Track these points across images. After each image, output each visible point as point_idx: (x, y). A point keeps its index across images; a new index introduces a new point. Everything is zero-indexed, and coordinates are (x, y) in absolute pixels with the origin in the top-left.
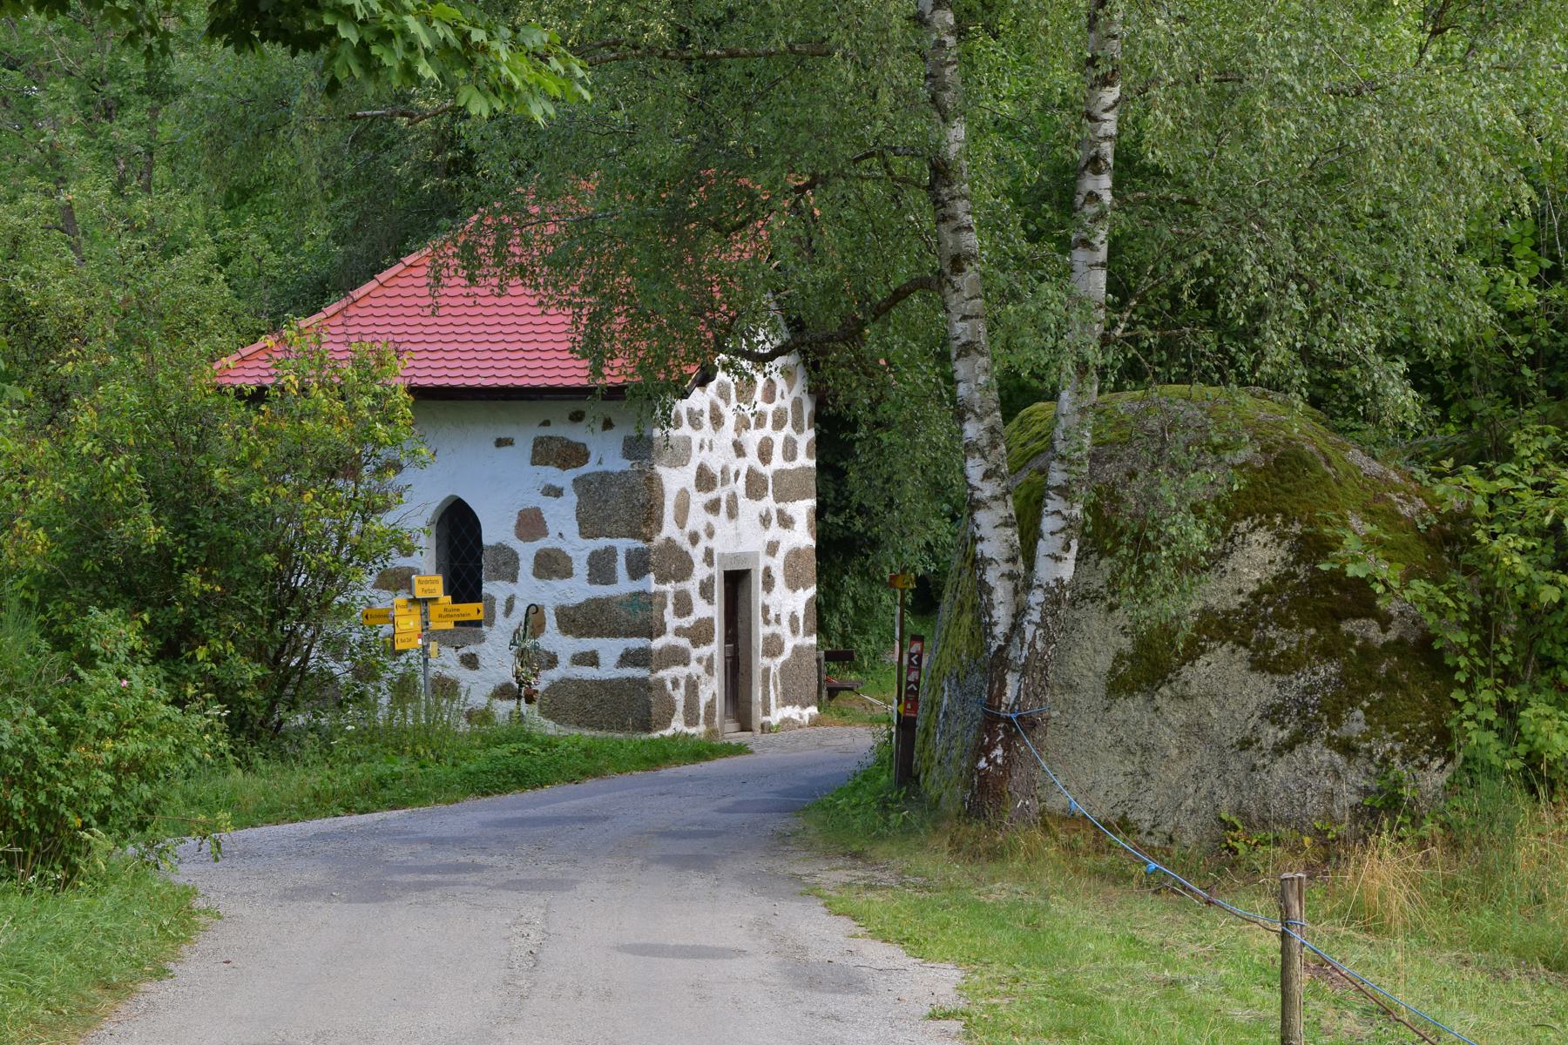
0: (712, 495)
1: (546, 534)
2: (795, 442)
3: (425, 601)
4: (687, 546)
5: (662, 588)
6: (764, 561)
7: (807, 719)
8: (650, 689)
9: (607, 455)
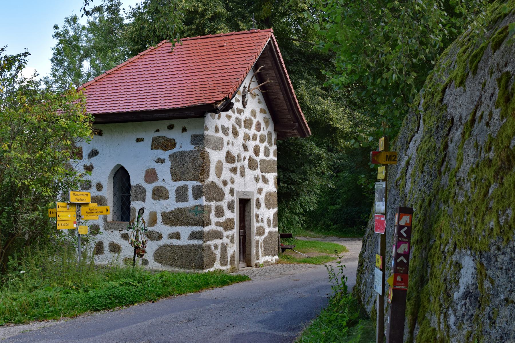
0: (233, 165)
1: (157, 180)
2: (269, 149)
3: (79, 205)
4: (221, 186)
5: (209, 204)
6: (256, 196)
7: (274, 261)
8: (203, 250)
9: (184, 143)
